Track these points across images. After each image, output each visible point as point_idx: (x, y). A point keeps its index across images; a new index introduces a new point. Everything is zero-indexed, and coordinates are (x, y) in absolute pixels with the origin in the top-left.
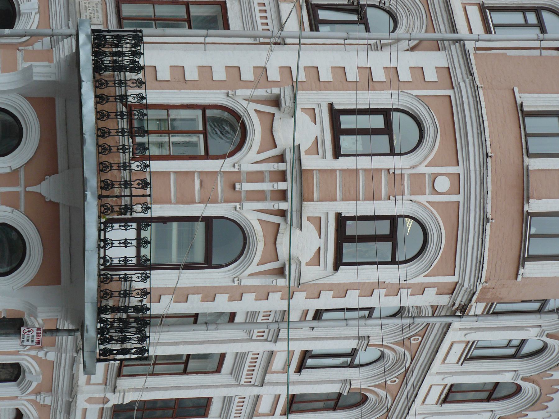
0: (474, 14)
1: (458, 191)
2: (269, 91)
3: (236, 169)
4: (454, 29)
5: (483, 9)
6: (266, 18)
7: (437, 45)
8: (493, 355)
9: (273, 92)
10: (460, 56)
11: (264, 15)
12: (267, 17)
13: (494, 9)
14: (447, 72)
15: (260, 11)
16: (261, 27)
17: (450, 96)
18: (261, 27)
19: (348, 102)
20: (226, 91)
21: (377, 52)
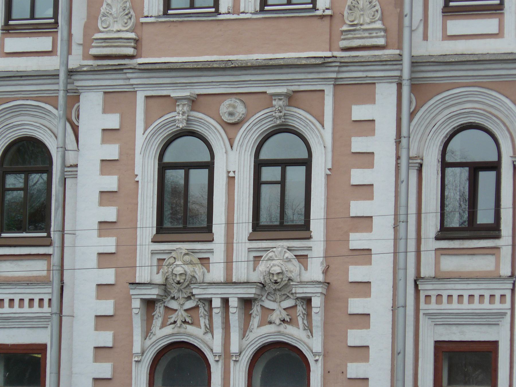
0: (13, 44)
1: (369, 123)
2: (135, 311)
3: (320, 358)
4: (55, 76)
5: (9, 29)
6: (22, 300)
7: (73, 98)
8: (259, 76)
9: (236, 306)
10: (107, 77)
11: (26, 302)
12: (491, 296)
13: (8, 16)
14: (113, 100)
15: (21, 305)
16: (46, 308)
17: (147, 97)
18: (46, 308)
19: (151, 219)
20: (134, 363)
21: (79, 173)
